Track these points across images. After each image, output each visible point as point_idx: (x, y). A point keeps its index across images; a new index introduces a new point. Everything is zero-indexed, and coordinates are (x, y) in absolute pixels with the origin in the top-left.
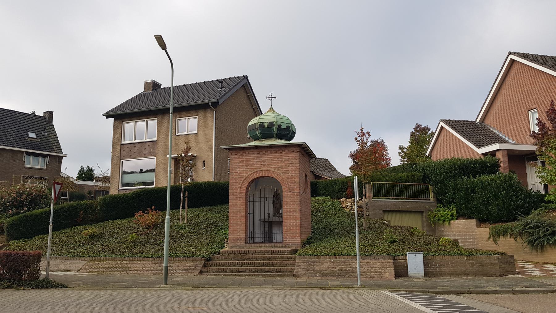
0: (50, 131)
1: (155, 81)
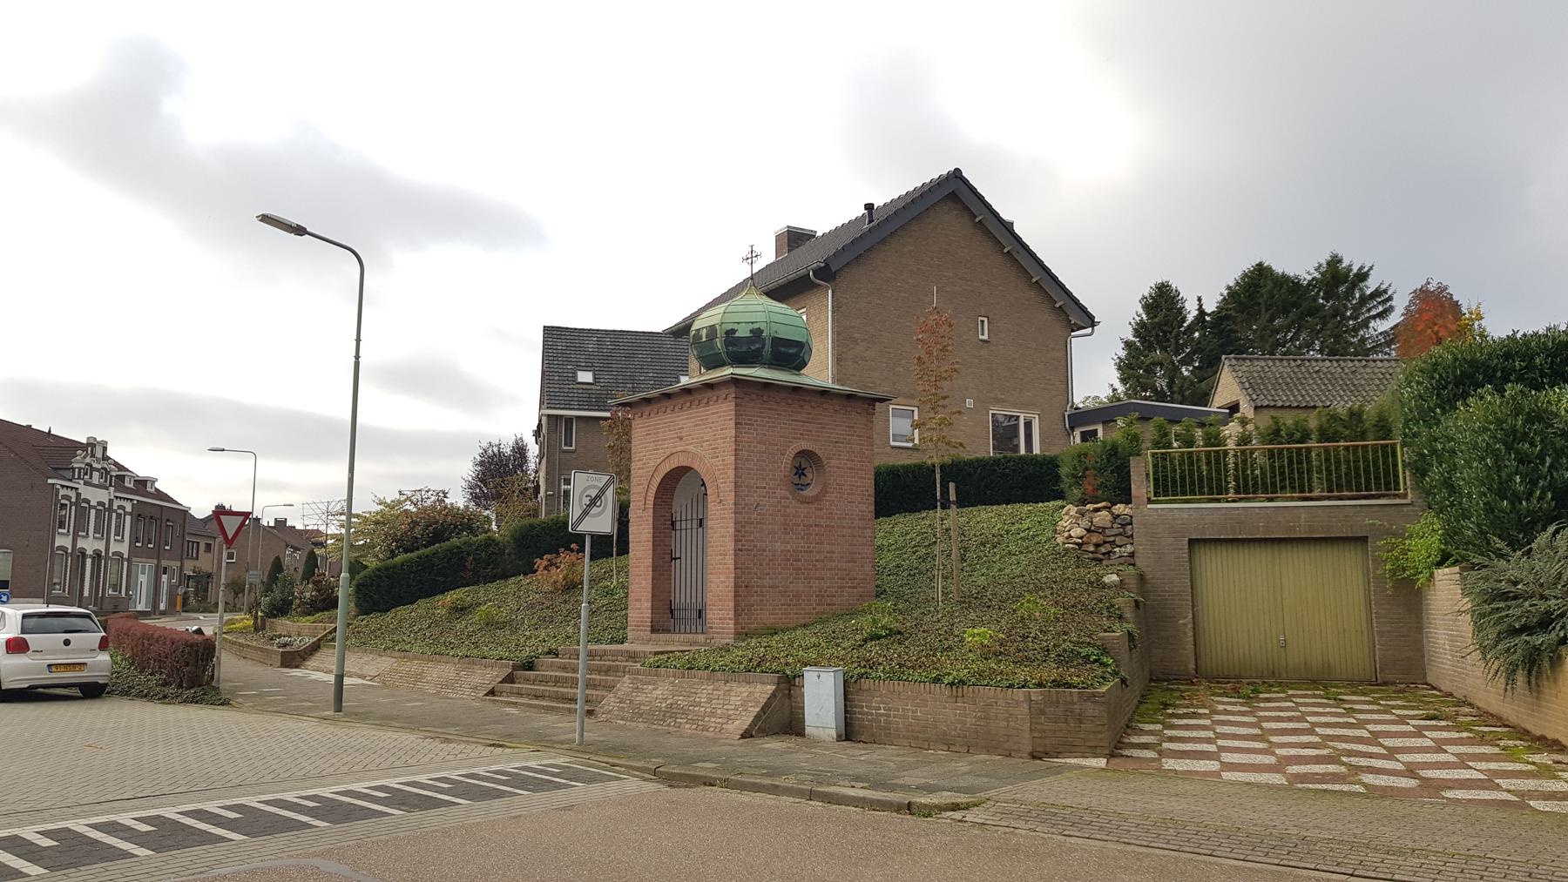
0: (562, 386)
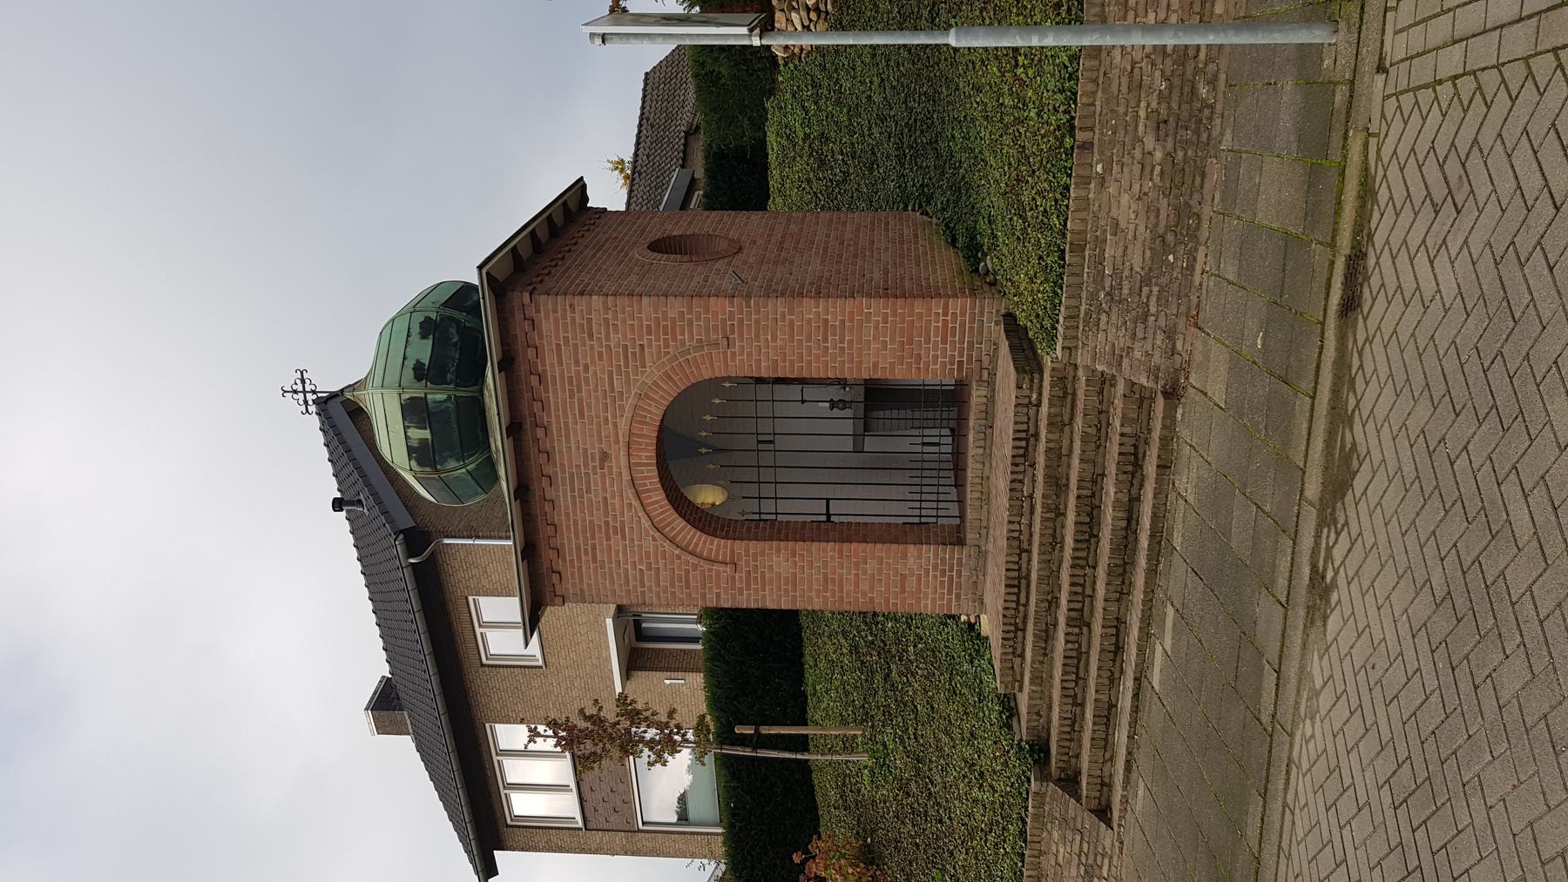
1: (370, 702)
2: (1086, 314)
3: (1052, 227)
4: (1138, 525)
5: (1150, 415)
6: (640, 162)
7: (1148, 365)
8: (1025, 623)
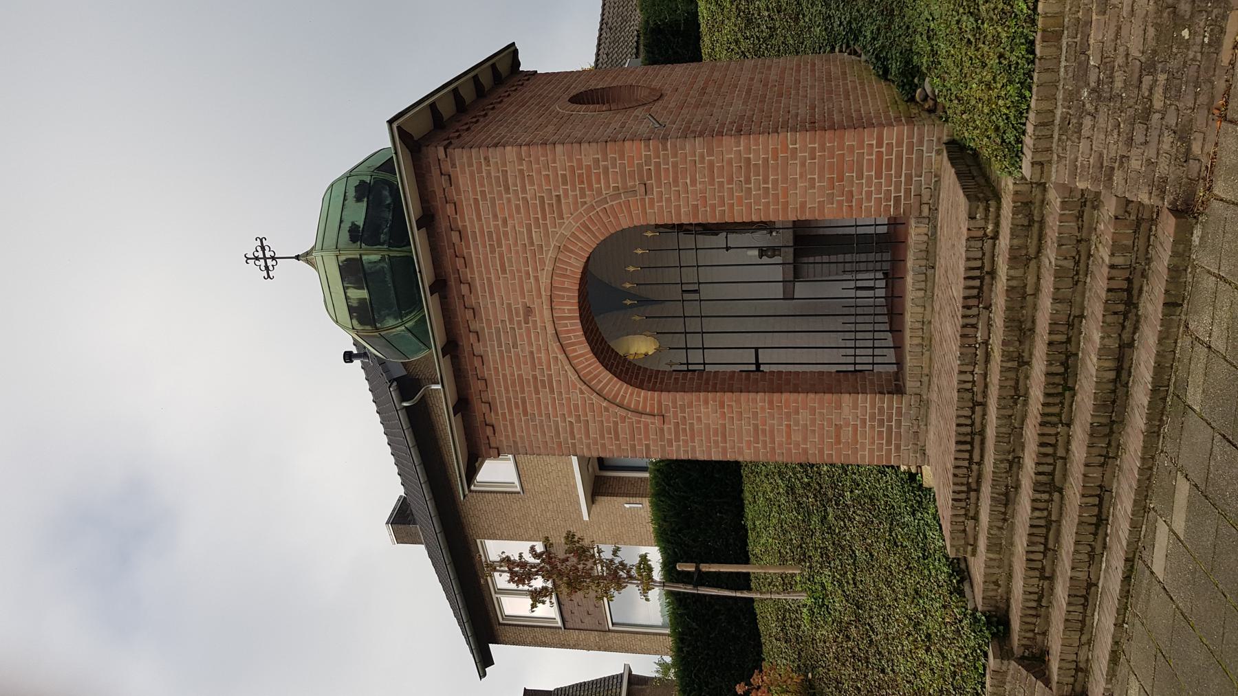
1: (390, 517)
2: (1063, 119)
3: (1016, 15)
4: (1130, 376)
5: (1149, 241)
6: (601, 60)
7: (1151, 177)
8: (978, 482)
